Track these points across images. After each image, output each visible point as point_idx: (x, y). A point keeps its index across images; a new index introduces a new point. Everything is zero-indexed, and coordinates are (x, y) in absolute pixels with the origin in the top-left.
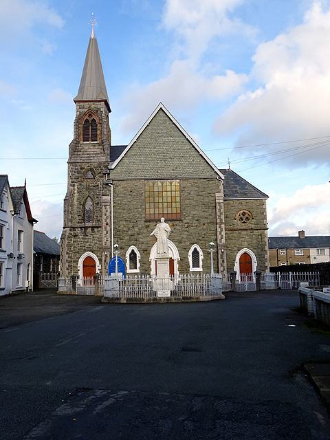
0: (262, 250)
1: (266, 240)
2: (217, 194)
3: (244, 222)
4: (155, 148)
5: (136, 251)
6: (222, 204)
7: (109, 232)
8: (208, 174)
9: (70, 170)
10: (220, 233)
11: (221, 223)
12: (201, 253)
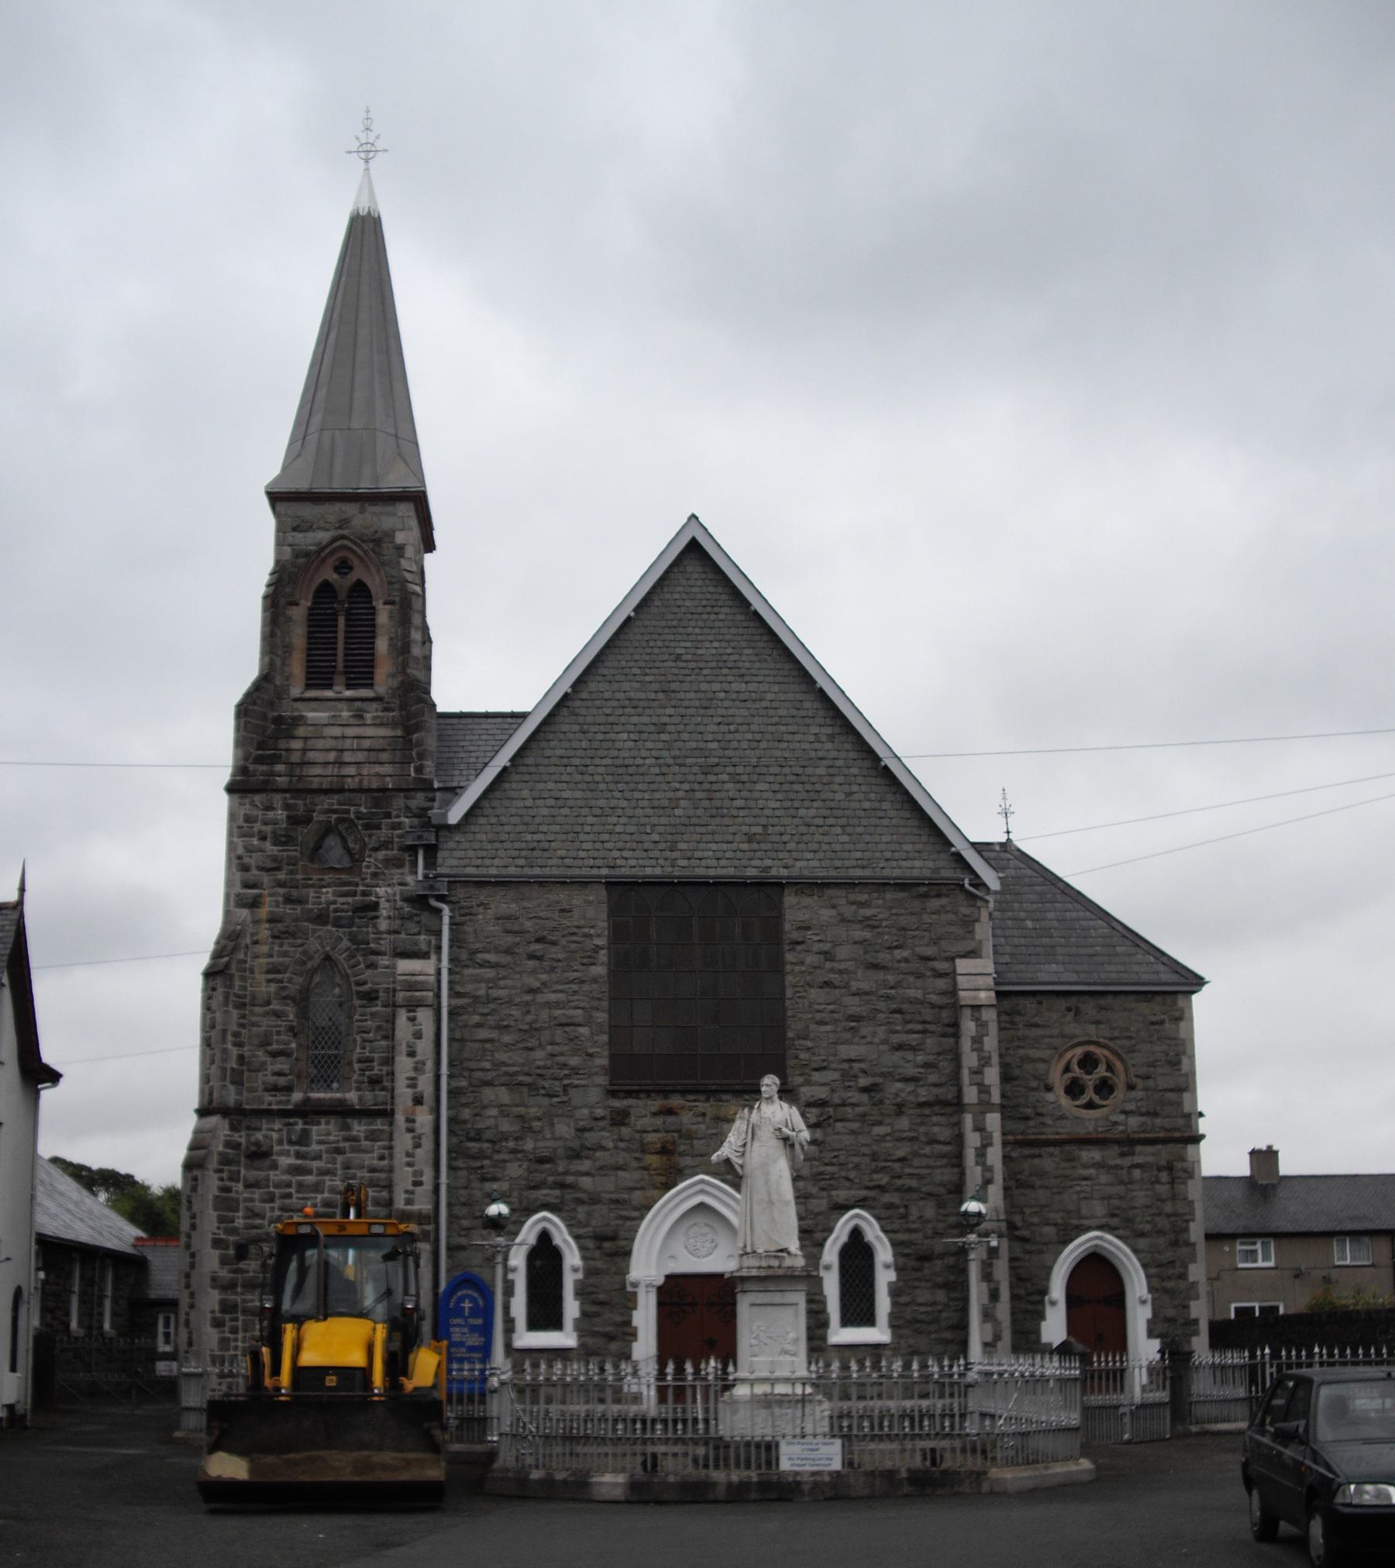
0: (1175, 1244)
1: (1194, 1191)
2: (962, 966)
3: (1090, 1105)
4: (661, 728)
5: (563, 1237)
6: (990, 1016)
7: (427, 1144)
8: (922, 866)
9: (240, 828)
10: (981, 1154)
11: (985, 1106)
12: (884, 1253)
